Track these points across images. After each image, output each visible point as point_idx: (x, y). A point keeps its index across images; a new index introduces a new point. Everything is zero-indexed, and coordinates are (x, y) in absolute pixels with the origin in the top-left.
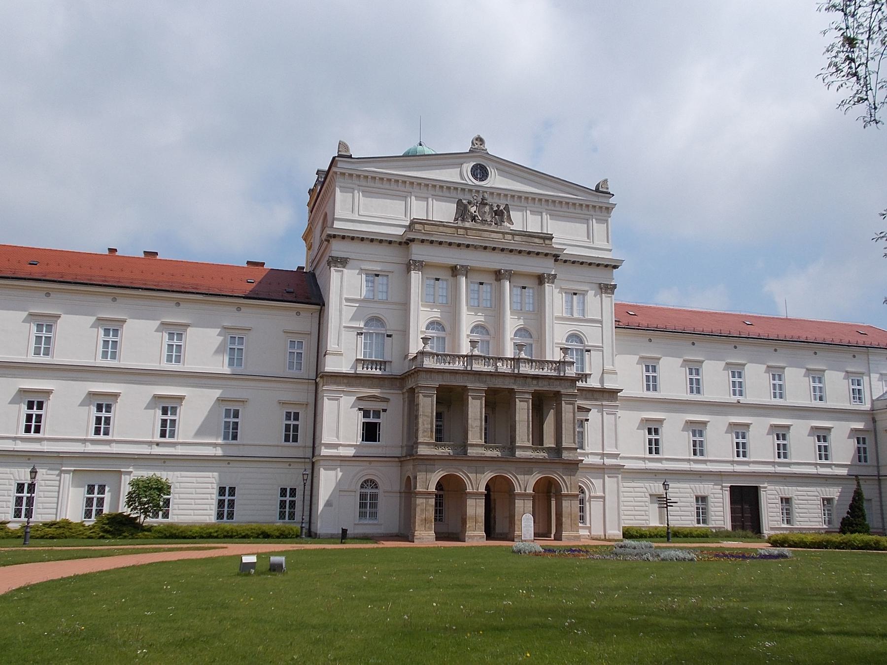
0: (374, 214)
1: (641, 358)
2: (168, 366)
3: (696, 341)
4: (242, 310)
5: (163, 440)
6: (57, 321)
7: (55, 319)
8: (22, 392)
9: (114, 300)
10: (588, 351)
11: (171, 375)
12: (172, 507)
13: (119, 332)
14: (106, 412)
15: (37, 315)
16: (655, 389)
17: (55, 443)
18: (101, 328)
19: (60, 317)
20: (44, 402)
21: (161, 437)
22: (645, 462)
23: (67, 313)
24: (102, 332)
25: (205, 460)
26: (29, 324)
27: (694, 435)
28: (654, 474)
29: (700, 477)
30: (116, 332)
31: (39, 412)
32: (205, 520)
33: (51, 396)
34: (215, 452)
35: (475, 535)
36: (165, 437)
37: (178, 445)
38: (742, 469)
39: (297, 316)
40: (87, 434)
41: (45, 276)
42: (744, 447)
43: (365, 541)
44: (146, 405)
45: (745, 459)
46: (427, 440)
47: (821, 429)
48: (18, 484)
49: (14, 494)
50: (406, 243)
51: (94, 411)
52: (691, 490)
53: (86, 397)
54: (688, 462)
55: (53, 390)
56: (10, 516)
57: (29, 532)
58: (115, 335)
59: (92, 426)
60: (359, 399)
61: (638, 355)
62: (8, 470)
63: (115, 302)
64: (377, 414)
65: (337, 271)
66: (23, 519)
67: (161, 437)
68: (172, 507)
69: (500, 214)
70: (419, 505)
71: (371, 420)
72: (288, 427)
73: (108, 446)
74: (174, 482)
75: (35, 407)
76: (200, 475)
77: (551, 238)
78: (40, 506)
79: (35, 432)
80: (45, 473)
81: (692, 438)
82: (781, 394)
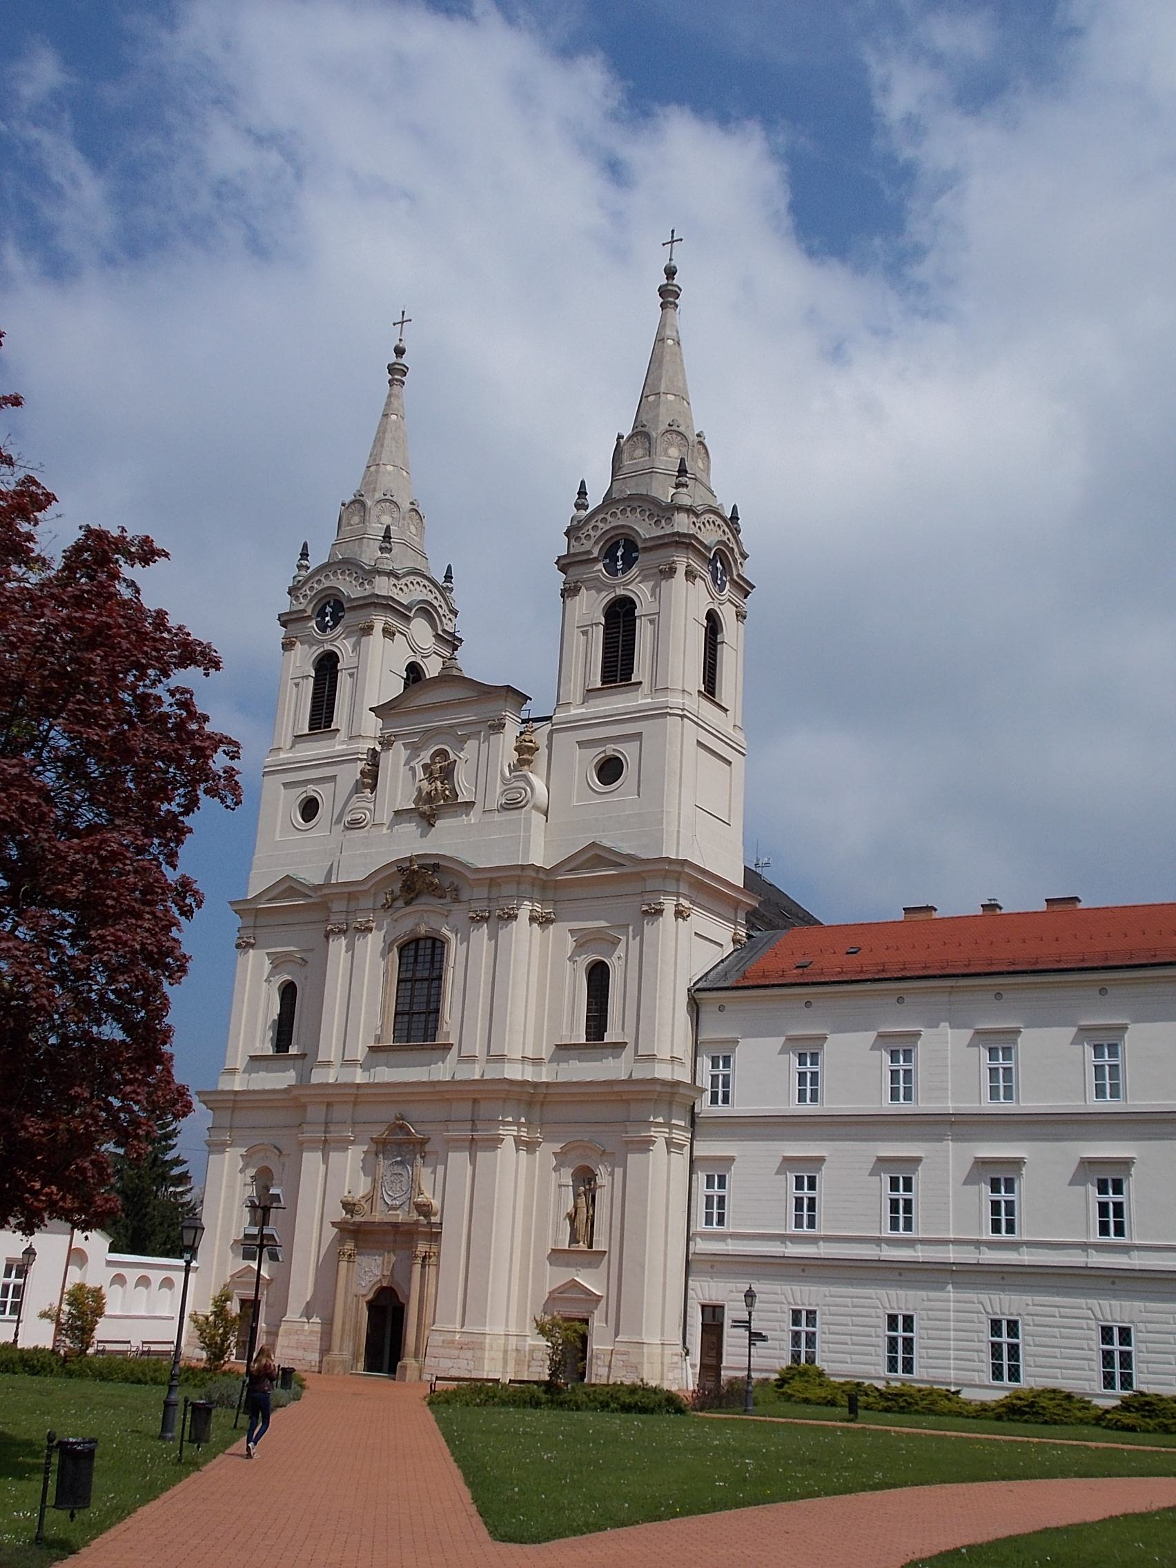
1: (790, 1039)
2: (1109, 1105)
3: (1002, 990)
4: (1004, 997)
6: (822, 1046)
7: (913, 1039)
8: (1086, 1164)
9: (1103, 991)
11: (1110, 1122)
12: (1024, 1360)
13: (1013, 1051)
14: (809, 1189)
15: (1003, 1032)
16: (1116, 1093)
17: (935, 1248)
18: (1087, 1044)
19: (1127, 1028)
20: (1015, 1179)
22: (881, 1247)
23: (1136, 1021)
24: (1090, 1051)
25: (1129, 1277)
26: (1081, 1047)
27: (995, 1189)
28: (710, 1264)
29: (1003, 1278)
30: (1007, 1051)
32: (946, 1378)
33: (1024, 1169)
34: (1085, 1259)
37: (1133, 1251)
38: (798, 1253)
39: (996, 1001)
40: (1088, 1235)
41: (1155, 956)
44: (776, 1170)
45: (1119, 1240)
47: (1107, 1163)
48: (992, 1321)
49: (1098, 1345)
51: (987, 1193)
52: (1090, 1312)
53: (1078, 1166)
54: (1083, 1250)
55: (1133, 1158)
56: (1097, 1386)
57: (751, 1392)
58: (1113, 1054)
59: (987, 1218)
61: (971, 1028)
62: (1082, 1301)
63: (1002, 1001)
68: (1024, 1360)
73: (815, 1246)
74: (1135, 1320)
75: (1111, 1191)
76: (1048, 1301)
78: (1030, 1360)
79: (809, 1227)
80: (1030, 1303)
81: (888, 1193)
82: (1008, 1090)
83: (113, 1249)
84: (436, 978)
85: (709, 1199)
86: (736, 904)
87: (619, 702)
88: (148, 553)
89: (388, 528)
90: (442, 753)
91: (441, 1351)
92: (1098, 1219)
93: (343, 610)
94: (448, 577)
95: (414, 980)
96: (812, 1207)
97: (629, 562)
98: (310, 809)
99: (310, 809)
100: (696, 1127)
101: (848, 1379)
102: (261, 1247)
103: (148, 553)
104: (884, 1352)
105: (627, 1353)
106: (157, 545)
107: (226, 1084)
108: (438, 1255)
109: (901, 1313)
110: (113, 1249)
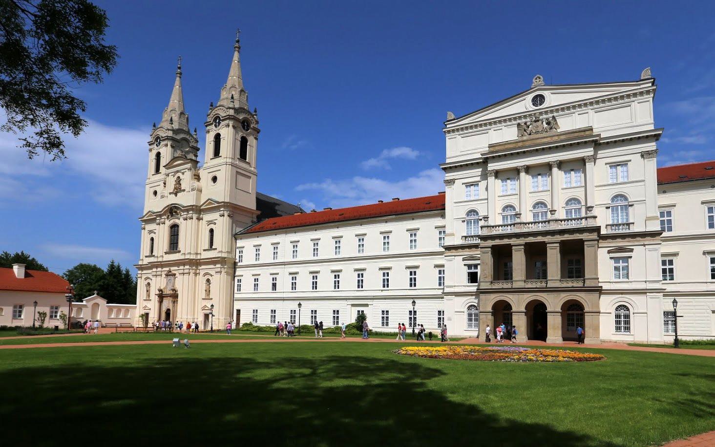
0: (469, 148)
5: (384, 289)
10: (632, 205)
21: (712, 278)
31: (411, 277)
35: (521, 336)
36: (385, 287)
42: (415, 280)
43: (454, 337)
46: (520, 278)
50: (485, 161)
60: (464, 260)
64: (476, 266)
65: (448, 188)
66: (336, 325)
67: (712, 278)
69: (552, 124)
70: (481, 319)
71: (473, 270)
72: (411, 279)
77: (592, 130)
92: (438, 281)
98: (215, 179)
107: (140, 263)
108: (177, 301)
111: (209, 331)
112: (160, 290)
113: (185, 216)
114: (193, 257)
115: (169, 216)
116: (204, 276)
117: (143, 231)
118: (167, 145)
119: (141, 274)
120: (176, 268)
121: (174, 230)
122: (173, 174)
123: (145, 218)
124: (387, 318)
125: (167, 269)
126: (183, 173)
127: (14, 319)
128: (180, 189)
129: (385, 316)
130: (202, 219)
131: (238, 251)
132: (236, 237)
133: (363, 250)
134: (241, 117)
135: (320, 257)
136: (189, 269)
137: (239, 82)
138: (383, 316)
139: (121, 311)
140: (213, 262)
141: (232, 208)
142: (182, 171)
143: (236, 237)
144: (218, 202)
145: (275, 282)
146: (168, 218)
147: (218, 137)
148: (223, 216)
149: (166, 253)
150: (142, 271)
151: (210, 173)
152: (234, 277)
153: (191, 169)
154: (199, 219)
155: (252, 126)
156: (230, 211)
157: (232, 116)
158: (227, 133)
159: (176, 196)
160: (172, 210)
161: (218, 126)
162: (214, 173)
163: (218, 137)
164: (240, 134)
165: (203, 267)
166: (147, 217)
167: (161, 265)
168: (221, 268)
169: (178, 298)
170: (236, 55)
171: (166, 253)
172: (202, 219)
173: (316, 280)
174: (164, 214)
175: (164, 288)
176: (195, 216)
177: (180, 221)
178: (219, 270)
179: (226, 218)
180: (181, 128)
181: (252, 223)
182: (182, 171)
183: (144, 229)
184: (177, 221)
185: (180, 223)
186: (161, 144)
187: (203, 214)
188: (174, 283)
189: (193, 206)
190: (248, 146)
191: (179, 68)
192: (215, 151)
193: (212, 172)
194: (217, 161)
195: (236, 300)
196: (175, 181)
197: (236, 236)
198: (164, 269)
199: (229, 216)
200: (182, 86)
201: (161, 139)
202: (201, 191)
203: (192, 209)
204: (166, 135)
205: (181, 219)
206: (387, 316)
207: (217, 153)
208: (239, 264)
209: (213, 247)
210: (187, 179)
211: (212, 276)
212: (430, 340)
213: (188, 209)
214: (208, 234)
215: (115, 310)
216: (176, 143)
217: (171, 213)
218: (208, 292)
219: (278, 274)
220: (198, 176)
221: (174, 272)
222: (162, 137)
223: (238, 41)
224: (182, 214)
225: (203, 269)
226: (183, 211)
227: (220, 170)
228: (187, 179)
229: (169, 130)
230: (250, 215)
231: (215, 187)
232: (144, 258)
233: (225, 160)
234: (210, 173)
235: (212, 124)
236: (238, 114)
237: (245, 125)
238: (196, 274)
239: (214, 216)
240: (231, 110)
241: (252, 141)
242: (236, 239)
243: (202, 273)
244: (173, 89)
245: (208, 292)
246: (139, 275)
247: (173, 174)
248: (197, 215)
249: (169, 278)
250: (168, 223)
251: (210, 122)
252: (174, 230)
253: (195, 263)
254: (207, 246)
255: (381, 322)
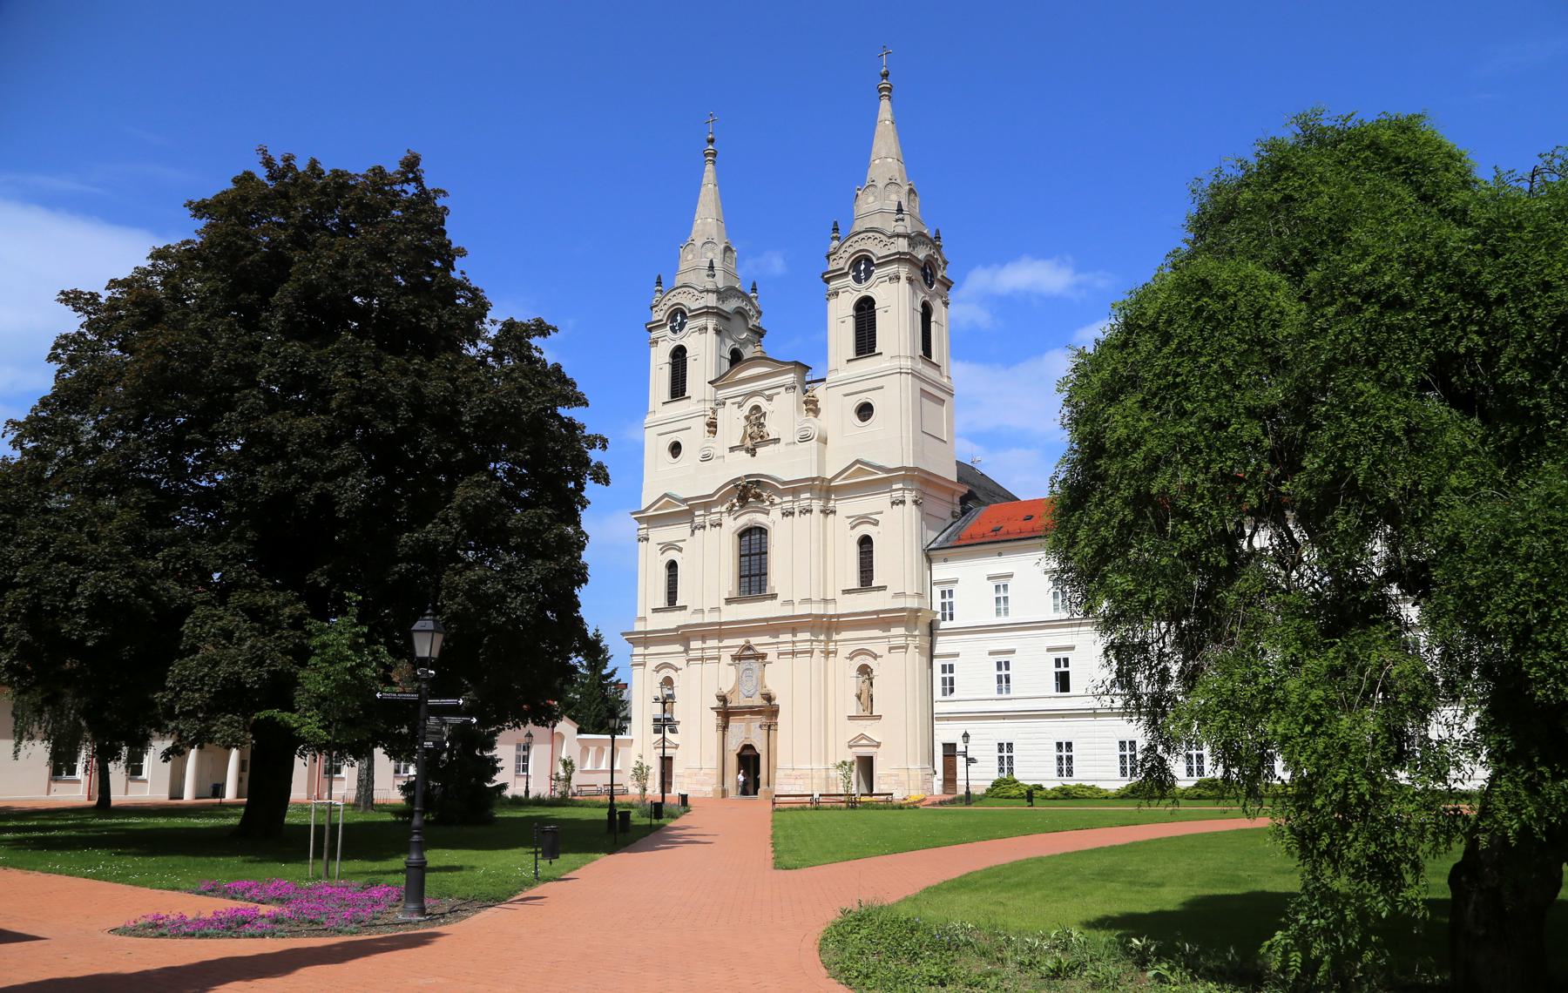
83: (580, 731)
84: (763, 553)
85: (944, 680)
86: (953, 493)
87: (868, 365)
88: (543, 329)
89: (711, 262)
90: (757, 408)
91: (785, 781)
93: (687, 318)
94: (754, 290)
95: (750, 555)
96: (1008, 681)
97: (869, 274)
98: (676, 449)
99: (676, 449)
100: (934, 637)
101: (1079, 783)
102: (664, 726)
103: (543, 329)
104: (1118, 765)
105: (898, 775)
106: (548, 322)
107: (639, 627)
108: (776, 724)
109: (1127, 740)
110: (580, 731)
111: (960, 799)
112: (723, 699)
113: (788, 506)
114: (817, 609)
115: (733, 505)
116: (658, 672)
117: (642, 545)
118: (706, 329)
119: (645, 655)
120: (766, 639)
121: (753, 546)
122: (739, 399)
123: (651, 513)
124: (1010, 758)
125: (741, 641)
126: (770, 398)
127: (56, 781)
128: (762, 437)
129: (1005, 754)
130: (834, 512)
131: (937, 591)
132: (930, 555)
133: (1006, 610)
134: (921, 253)
135: (1014, 617)
136: (812, 641)
137: (900, 171)
138: (1123, 753)
139: (603, 750)
140: (882, 621)
141: (922, 483)
142: (767, 393)
143: (930, 555)
144: (685, 500)
145: (1062, 669)
146: (730, 511)
147: (679, 355)
148: (903, 502)
149: (729, 601)
150: (720, 641)
151: (878, 388)
152: (932, 657)
153: (794, 388)
154: (826, 512)
155: (939, 277)
156: (917, 490)
157: (713, 308)
158: (704, 349)
159: (754, 455)
160: (747, 492)
161: (866, 279)
162: (674, 434)
163: (679, 355)
164: (921, 296)
165: (845, 635)
166: (656, 510)
167: (720, 631)
168: (907, 636)
169: (776, 717)
170: (885, 109)
171: (729, 601)
172: (834, 512)
173: (1007, 672)
174: (721, 502)
175: (732, 691)
176: (817, 505)
177: (772, 519)
178: (901, 641)
179: (910, 510)
180: (729, 284)
181: (953, 517)
182: (767, 393)
183: (647, 539)
184: (759, 519)
185: (771, 525)
186: (687, 327)
187: (836, 500)
188: (763, 676)
189: (813, 479)
190: (933, 325)
191: (711, 141)
192: (672, 388)
193: (857, 393)
194: (680, 407)
195: (938, 719)
196: (747, 418)
197: (931, 553)
198: (727, 642)
199: (915, 502)
200: (720, 182)
201: (688, 315)
202: (826, 439)
203: (810, 489)
204: (701, 303)
205: (776, 513)
206: (1010, 754)
207: (678, 389)
208: (943, 625)
209: (678, 603)
210: (782, 412)
211: (677, 670)
212: (1032, 806)
213: (795, 489)
214: (663, 574)
215: (593, 750)
216: (723, 321)
217: (743, 499)
218: (866, 699)
219: (957, 655)
220: (815, 402)
221: (760, 650)
222: (691, 311)
223: (885, 75)
224: (777, 500)
225: (847, 641)
226: (781, 493)
227: (882, 388)
228: (782, 412)
229: (708, 291)
230: (949, 498)
231: (676, 466)
232: (649, 614)
233: (896, 363)
234: (878, 388)
235: (846, 274)
236: (723, 302)
237: (927, 273)
238: (827, 653)
239: (877, 503)
240: (900, 239)
241: (939, 313)
242: (930, 561)
243: (843, 651)
244: (699, 192)
245: (866, 699)
246: (636, 660)
247: (739, 399)
248: (821, 503)
249: (744, 664)
250: (733, 524)
251: (661, 320)
252: (753, 546)
253: (827, 626)
254: (662, 602)
255: (1074, 765)
